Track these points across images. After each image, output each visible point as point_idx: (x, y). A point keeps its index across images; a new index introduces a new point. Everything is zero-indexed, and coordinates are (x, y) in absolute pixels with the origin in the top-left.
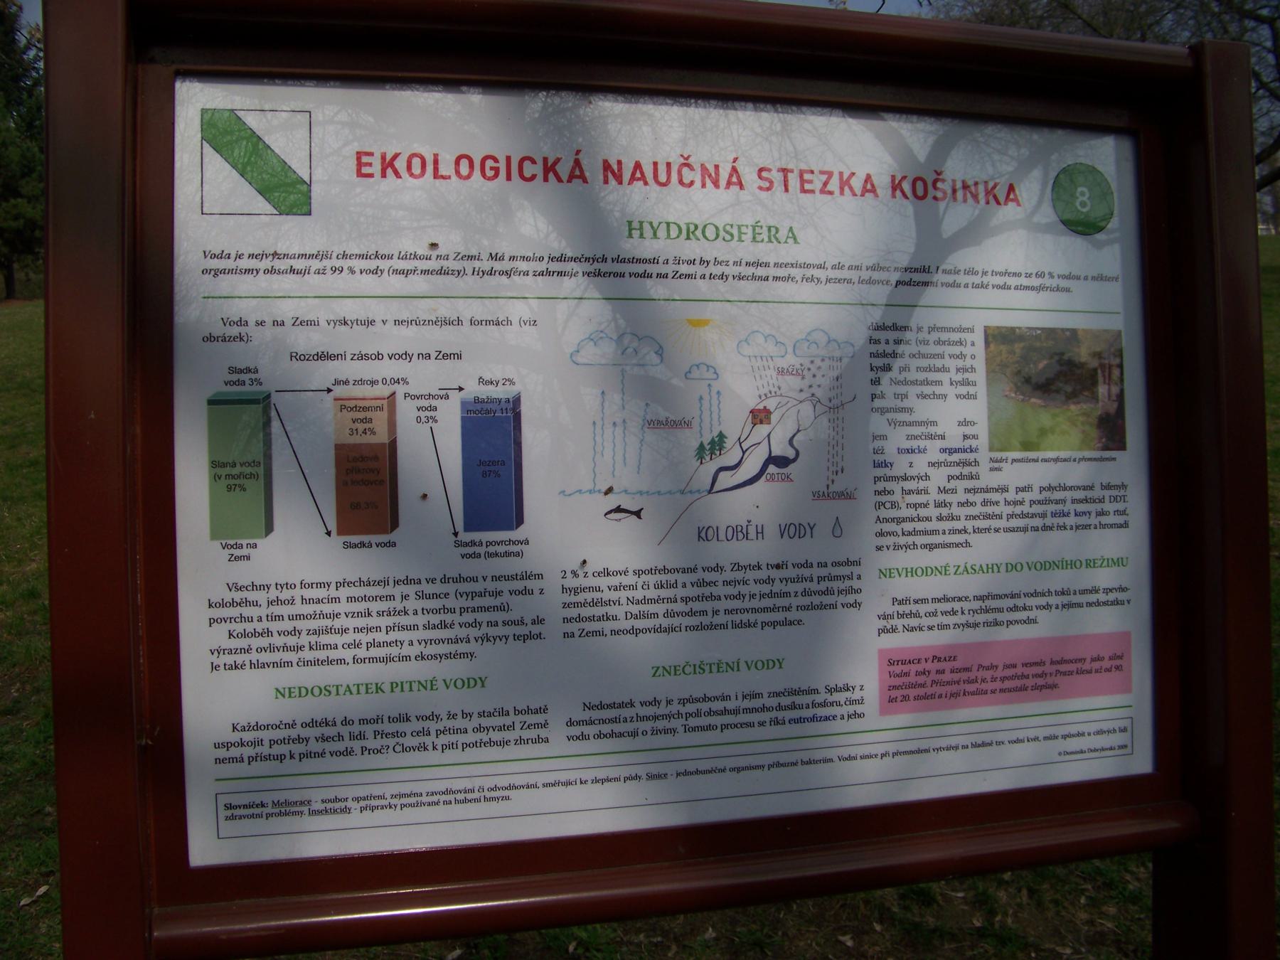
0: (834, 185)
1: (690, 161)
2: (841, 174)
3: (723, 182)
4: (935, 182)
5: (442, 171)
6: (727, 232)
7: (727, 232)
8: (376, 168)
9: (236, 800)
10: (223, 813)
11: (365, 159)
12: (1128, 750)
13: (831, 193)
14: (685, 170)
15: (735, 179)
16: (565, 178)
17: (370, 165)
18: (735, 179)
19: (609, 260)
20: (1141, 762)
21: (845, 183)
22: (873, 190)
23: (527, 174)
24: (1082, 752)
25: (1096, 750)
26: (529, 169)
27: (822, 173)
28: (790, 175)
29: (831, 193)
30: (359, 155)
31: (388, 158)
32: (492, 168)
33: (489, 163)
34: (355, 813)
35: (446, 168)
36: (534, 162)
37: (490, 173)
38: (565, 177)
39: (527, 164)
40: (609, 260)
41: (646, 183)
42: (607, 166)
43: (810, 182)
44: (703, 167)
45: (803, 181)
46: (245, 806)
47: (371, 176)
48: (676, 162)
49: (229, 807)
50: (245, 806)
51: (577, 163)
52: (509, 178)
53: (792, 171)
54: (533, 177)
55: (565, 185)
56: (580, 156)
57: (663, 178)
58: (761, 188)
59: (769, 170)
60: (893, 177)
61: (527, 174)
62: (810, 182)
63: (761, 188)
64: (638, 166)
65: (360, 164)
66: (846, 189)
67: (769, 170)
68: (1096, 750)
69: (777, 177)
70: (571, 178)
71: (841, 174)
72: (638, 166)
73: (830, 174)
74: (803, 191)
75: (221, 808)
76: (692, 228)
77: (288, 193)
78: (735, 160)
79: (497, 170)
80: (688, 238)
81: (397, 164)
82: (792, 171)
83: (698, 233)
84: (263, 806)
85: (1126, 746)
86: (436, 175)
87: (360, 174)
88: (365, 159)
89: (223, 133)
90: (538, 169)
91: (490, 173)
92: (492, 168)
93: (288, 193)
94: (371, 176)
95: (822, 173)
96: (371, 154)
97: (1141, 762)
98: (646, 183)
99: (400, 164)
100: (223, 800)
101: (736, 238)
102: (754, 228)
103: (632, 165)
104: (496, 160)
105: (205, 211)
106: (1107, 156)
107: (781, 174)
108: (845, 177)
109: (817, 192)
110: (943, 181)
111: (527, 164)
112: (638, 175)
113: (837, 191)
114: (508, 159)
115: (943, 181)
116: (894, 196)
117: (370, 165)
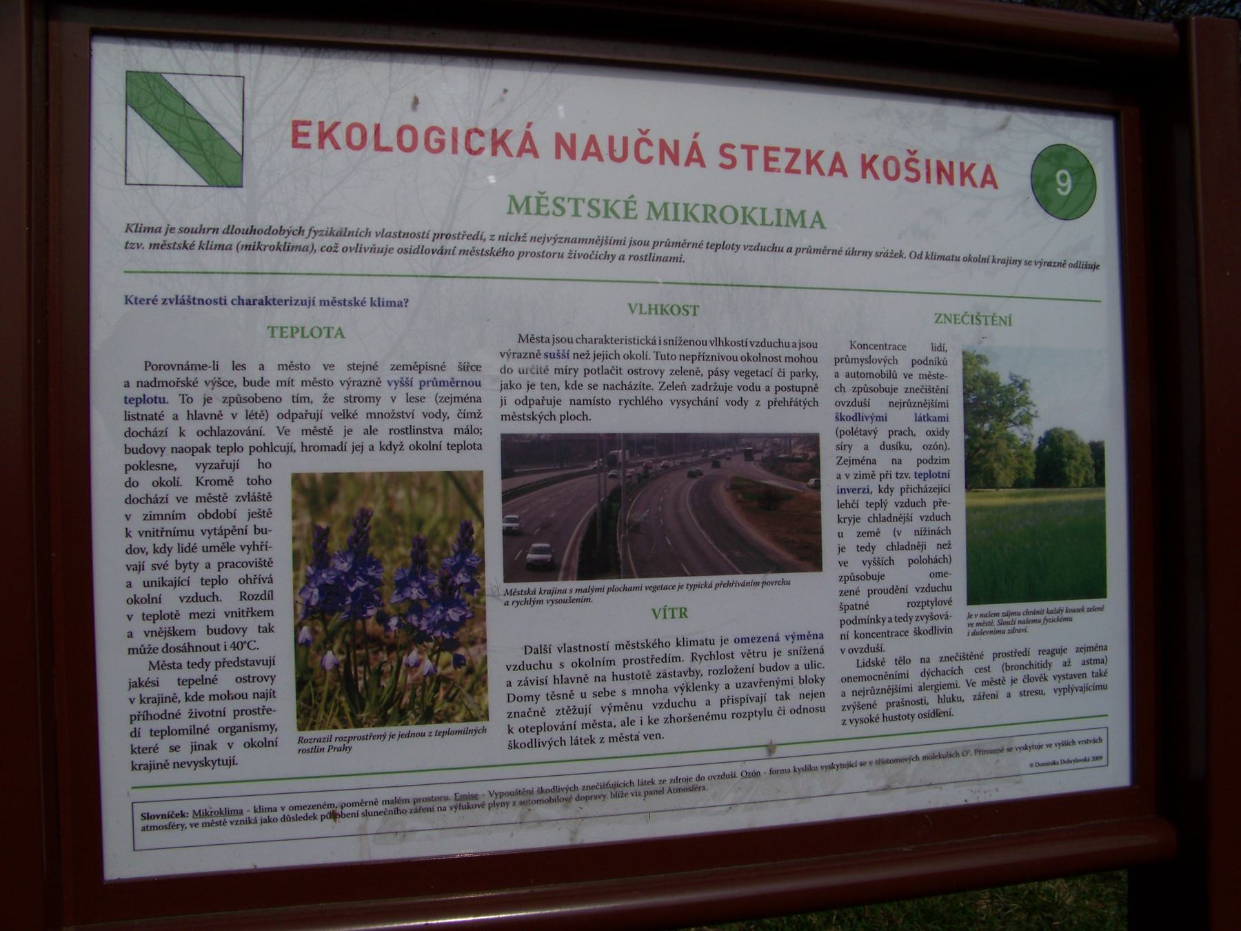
0: (801, 163)
1: (648, 136)
2: (808, 152)
3: (683, 157)
4: (908, 161)
5: (384, 143)
6: (558, 206)
7: (558, 206)
8: (313, 139)
9: (153, 809)
10: (140, 823)
11: (772, 154)
12: (1103, 762)
13: (798, 172)
14: (643, 145)
15: (696, 156)
16: (826, 171)
17: (306, 135)
18: (696, 156)
19: (373, 234)
20: (1114, 772)
21: (812, 162)
22: (993, 182)
23: (644, 156)
24: (1054, 763)
25: (1069, 762)
26: (476, 142)
27: (788, 150)
28: (754, 152)
29: (798, 172)
30: (296, 124)
31: (499, 135)
32: (437, 140)
33: (434, 135)
34: (451, 794)
35: (388, 138)
36: (482, 134)
37: (435, 146)
38: (826, 170)
39: (474, 136)
40: (373, 234)
41: (601, 159)
42: (559, 139)
43: (776, 160)
44: (663, 144)
45: (767, 159)
46: (164, 816)
47: (308, 146)
48: (633, 138)
49: (146, 816)
50: (164, 816)
51: (528, 136)
52: (455, 151)
53: (756, 148)
54: (650, 159)
55: (826, 178)
56: (531, 130)
57: (619, 153)
58: (722, 166)
59: (732, 147)
60: (863, 156)
61: (644, 156)
62: (776, 160)
63: (722, 166)
64: (592, 140)
65: (296, 135)
66: (814, 168)
67: (732, 147)
68: (1069, 762)
69: (741, 155)
70: (522, 151)
71: (808, 152)
72: (592, 140)
73: (796, 152)
74: (767, 169)
75: (138, 817)
76: (710, 210)
77: (217, 162)
78: (696, 135)
79: (442, 143)
80: (744, 223)
81: (820, 160)
82: (756, 148)
83: (717, 215)
84: (183, 815)
85: (1101, 758)
86: (378, 148)
87: (295, 145)
88: (301, 129)
89: (148, 95)
90: (486, 142)
91: (435, 146)
92: (437, 140)
93: (217, 162)
94: (308, 146)
95: (788, 150)
96: (309, 124)
97: (1114, 772)
98: (601, 159)
99: (339, 135)
100: (140, 809)
101: (603, 213)
102: (627, 203)
103: (586, 139)
104: (441, 132)
105: (137, 175)
106: (1093, 138)
107: (745, 152)
108: (813, 155)
109: (783, 170)
110: (916, 161)
111: (474, 136)
112: (838, 166)
113: (803, 169)
114: (455, 130)
115: (916, 161)
116: (864, 176)
117: (306, 135)
